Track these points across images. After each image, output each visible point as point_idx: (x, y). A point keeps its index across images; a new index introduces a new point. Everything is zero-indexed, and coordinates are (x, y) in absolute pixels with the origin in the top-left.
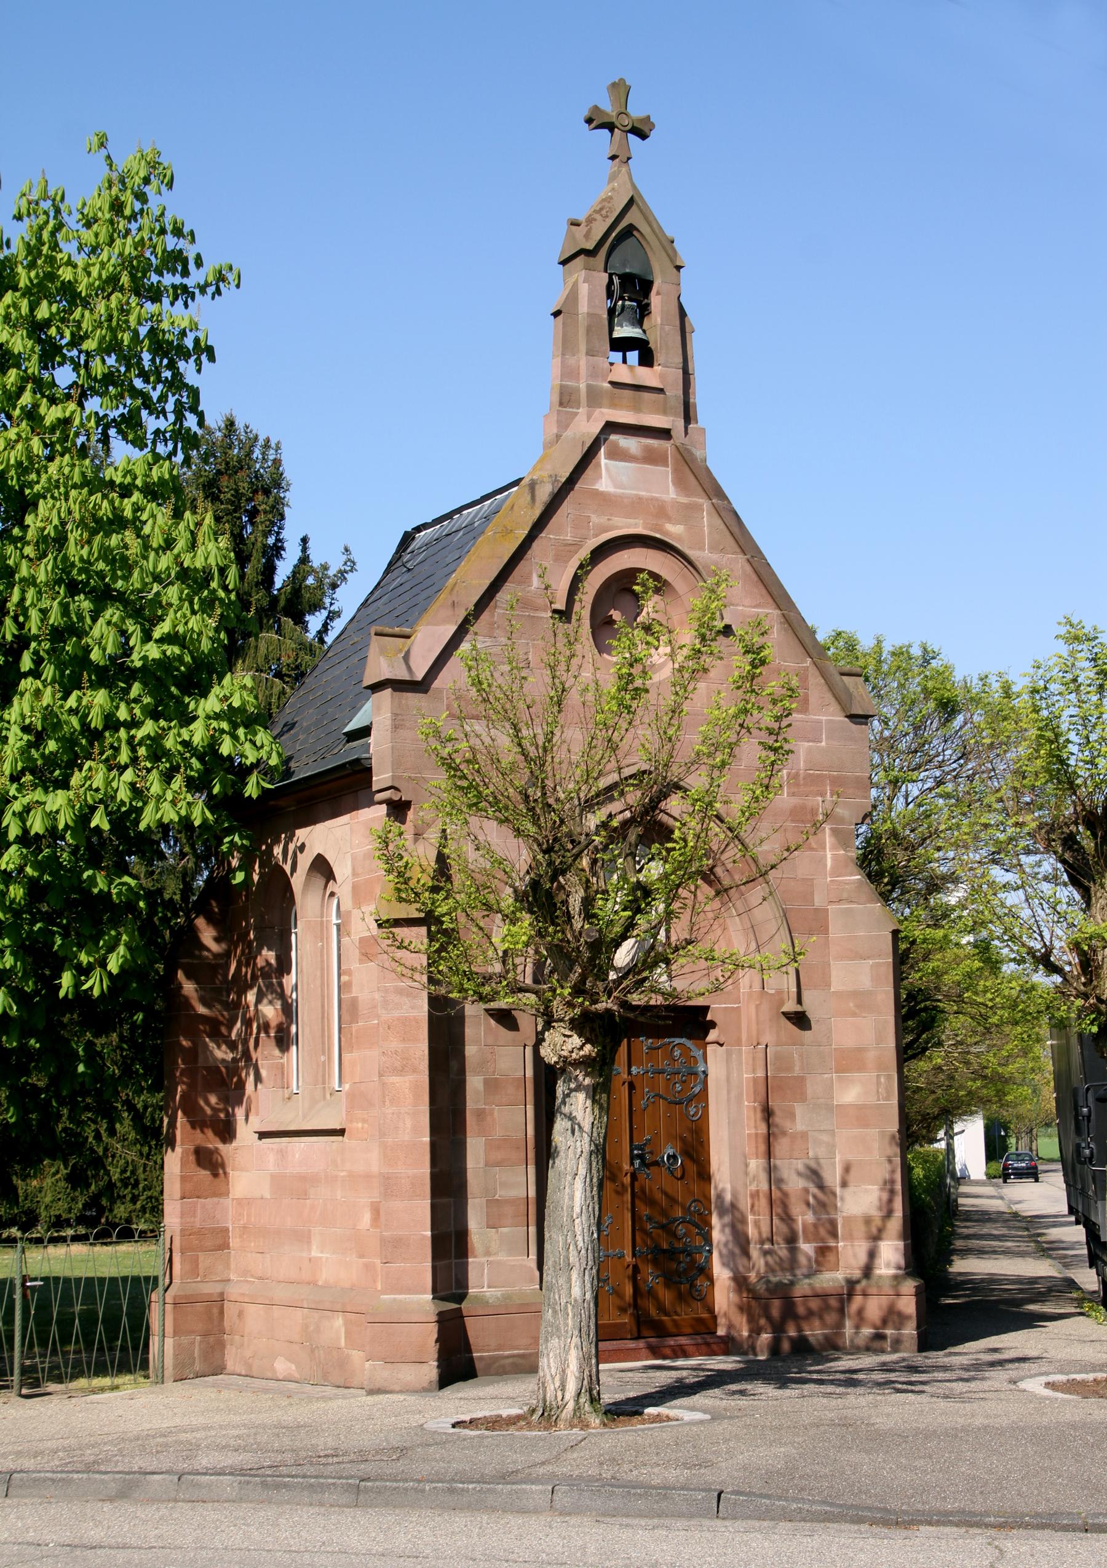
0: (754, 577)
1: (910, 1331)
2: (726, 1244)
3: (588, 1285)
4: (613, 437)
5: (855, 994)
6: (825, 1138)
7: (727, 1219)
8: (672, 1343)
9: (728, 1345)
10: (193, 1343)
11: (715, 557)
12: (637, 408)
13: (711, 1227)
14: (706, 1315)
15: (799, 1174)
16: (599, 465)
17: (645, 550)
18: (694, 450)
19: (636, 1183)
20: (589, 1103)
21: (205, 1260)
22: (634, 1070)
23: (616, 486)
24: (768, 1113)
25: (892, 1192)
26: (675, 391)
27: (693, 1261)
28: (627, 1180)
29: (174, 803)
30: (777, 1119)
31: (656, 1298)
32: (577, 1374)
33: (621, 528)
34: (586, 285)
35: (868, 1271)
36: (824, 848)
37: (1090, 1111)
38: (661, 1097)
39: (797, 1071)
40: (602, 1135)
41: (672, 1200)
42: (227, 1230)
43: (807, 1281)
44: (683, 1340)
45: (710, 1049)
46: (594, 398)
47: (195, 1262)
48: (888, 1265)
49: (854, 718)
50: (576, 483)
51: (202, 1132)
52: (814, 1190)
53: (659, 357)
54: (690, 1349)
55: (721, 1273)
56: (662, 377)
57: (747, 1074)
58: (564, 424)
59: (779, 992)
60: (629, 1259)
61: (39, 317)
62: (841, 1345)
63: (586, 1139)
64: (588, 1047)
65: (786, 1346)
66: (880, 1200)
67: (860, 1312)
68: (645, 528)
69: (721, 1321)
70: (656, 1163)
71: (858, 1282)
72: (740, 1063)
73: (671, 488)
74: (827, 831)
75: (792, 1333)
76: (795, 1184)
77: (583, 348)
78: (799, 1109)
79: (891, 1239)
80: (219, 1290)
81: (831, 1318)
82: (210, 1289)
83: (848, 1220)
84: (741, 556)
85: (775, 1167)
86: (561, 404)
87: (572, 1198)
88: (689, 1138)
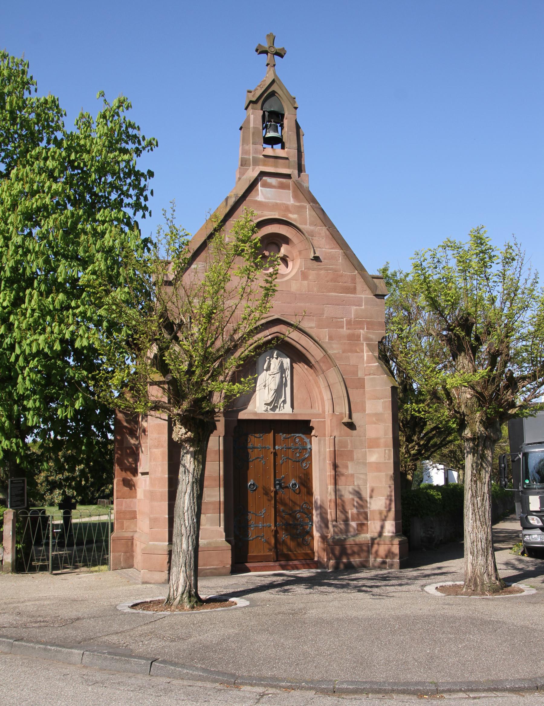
0: (331, 236)
1: (397, 560)
2: (318, 522)
3: (190, 543)
4: (264, 178)
5: (376, 415)
6: (362, 476)
7: (318, 512)
8: (291, 563)
9: (318, 564)
10: (120, 556)
11: (312, 228)
12: (276, 166)
13: (312, 515)
14: (309, 552)
15: (350, 493)
16: (258, 190)
17: (279, 225)
18: (303, 183)
19: (278, 496)
20: (192, 459)
21: (126, 523)
22: (277, 447)
23: (265, 198)
24: (335, 466)
25: (391, 500)
26: (294, 159)
27: (304, 529)
28: (273, 494)
29: (88, 338)
30: (341, 469)
31: (287, 545)
32: (183, 584)
33: (266, 216)
34: (252, 116)
35: (380, 534)
36: (363, 352)
37: (505, 466)
38: (289, 459)
39: (349, 448)
40: (199, 474)
41: (295, 503)
42: (136, 511)
43: (353, 538)
44: (296, 562)
45: (313, 438)
46: (256, 162)
47: (122, 524)
48: (389, 532)
49: (377, 296)
50: (247, 197)
51: (126, 472)
52: (356, 499)
53: (287, 145)
54: (299, 566)
55: (316, 534)
56: (287, 153)
57: (329, 449)
58: (242, 173)
59: (341, 414)
60: (273, 528)
61: (71, 159)
62: (368, 565)
63: (191, 476)
64: (189, 433)
65: (342, 566)
66: (386, 504)
67: (377, 552)
68: (279, 216)
69: (316, 554)
70: (287, 487)
71: (376, 539)
72: (325, 444)
73: (292, 199)
74: (365, 344)
75: (345, 560)
76: (348, 496)
77: (251, 142)
78: (350, 464)
79: (390, 520)
80: (131, 535)
81: (364, 555)
82: (128, 535)
83: (373, 512)
84: (324, 227)
85: (339, 490)
86: (242, 165)
87: (184, 503)
88: (303, 477)
